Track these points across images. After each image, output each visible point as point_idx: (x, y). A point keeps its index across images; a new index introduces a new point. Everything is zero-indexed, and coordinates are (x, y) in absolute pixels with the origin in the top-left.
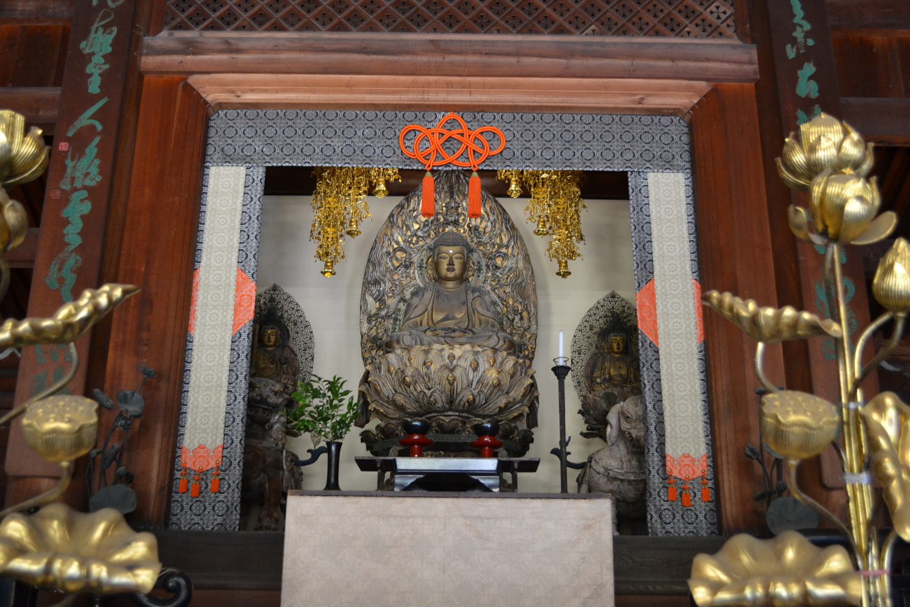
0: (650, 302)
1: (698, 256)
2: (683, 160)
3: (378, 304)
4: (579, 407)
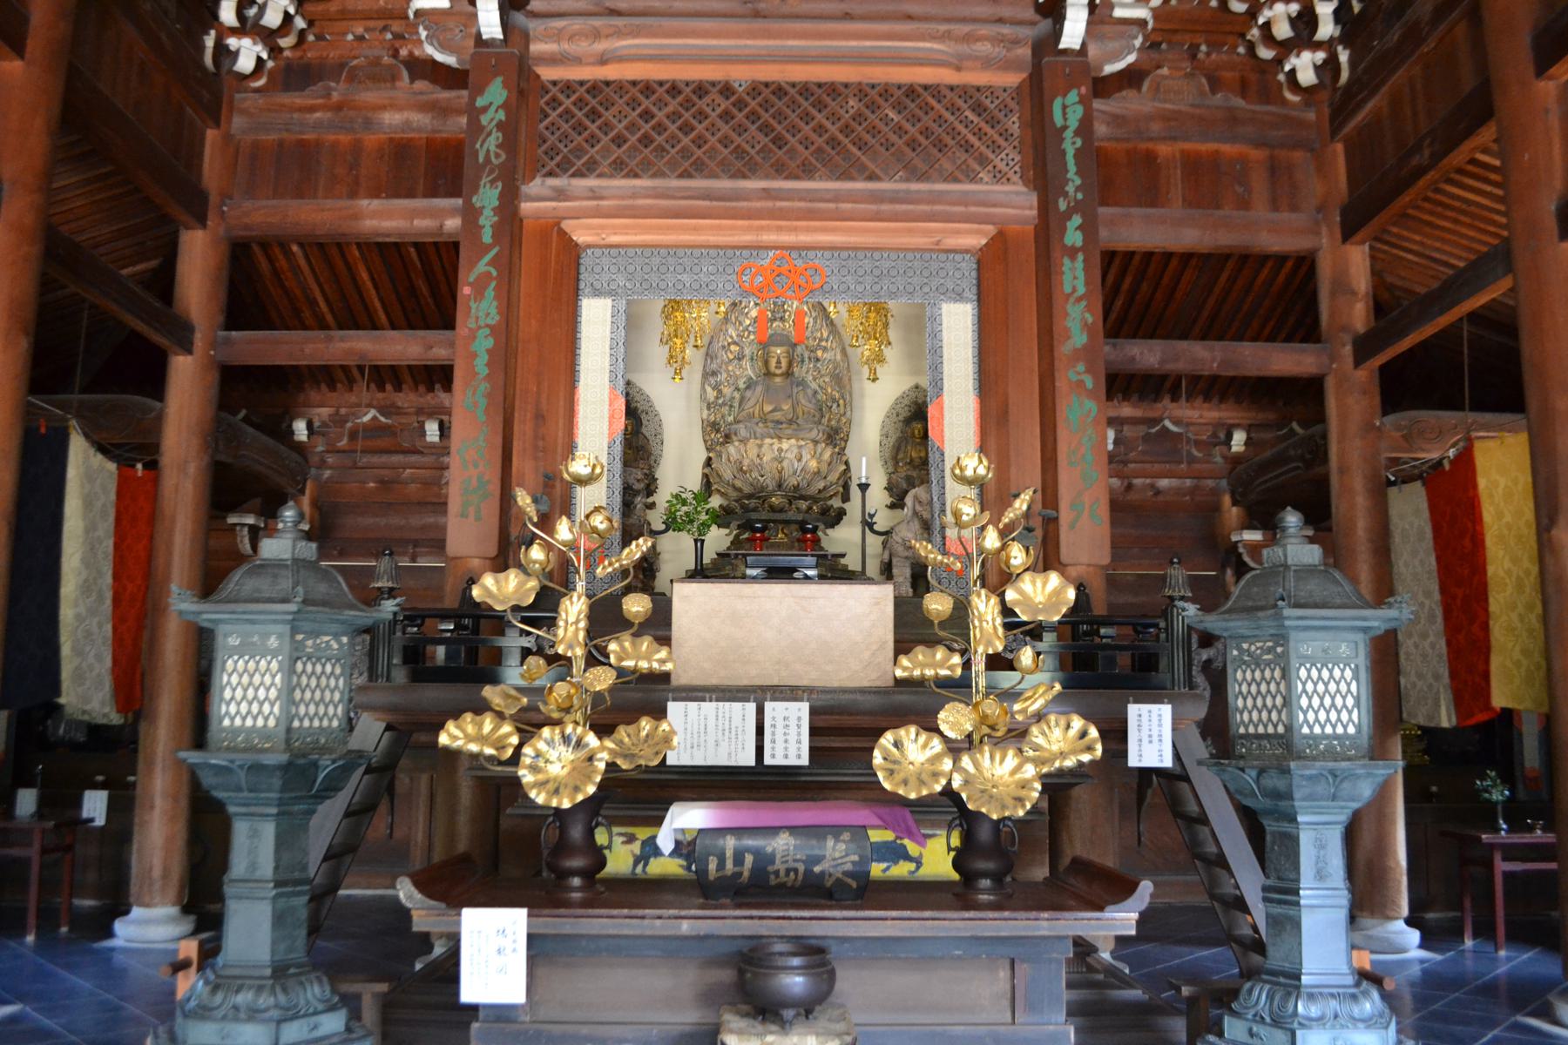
2: (971, 293)
4: (884, 484)
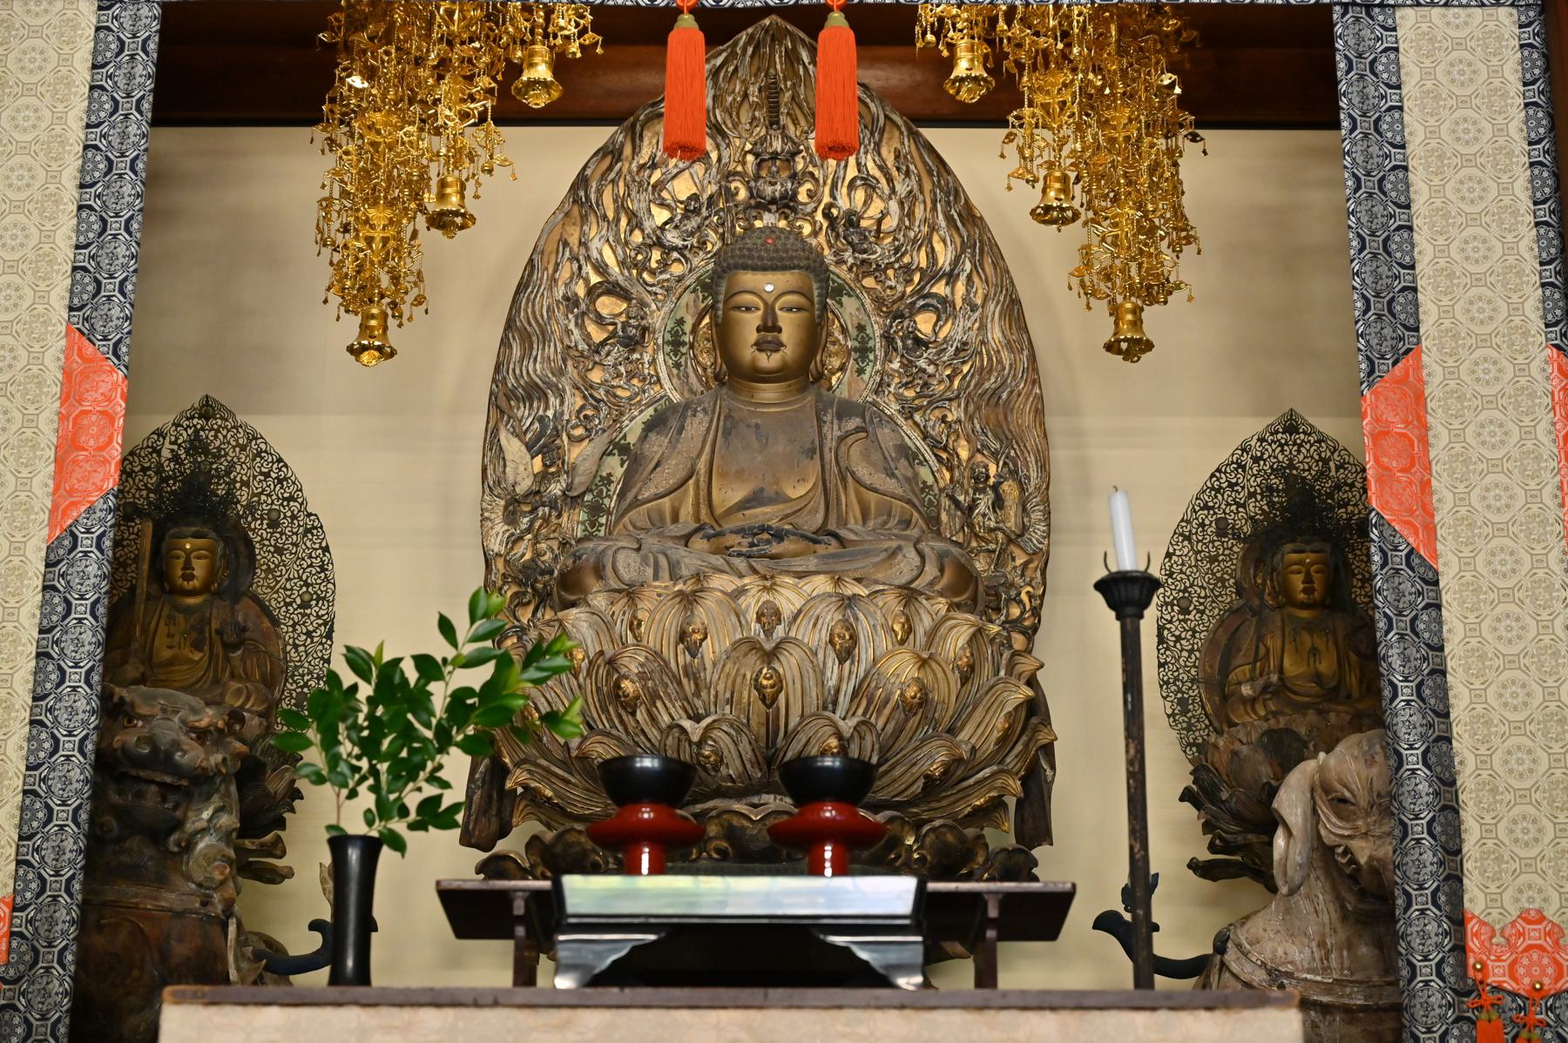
0: (1407, 423)
1: (1557, 153)
3: (538, 464)
